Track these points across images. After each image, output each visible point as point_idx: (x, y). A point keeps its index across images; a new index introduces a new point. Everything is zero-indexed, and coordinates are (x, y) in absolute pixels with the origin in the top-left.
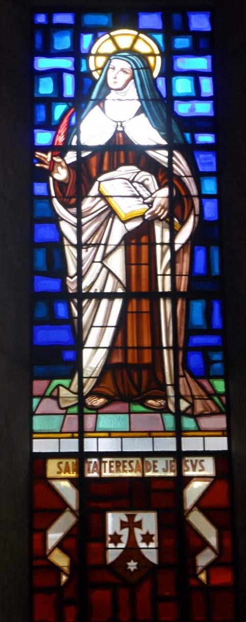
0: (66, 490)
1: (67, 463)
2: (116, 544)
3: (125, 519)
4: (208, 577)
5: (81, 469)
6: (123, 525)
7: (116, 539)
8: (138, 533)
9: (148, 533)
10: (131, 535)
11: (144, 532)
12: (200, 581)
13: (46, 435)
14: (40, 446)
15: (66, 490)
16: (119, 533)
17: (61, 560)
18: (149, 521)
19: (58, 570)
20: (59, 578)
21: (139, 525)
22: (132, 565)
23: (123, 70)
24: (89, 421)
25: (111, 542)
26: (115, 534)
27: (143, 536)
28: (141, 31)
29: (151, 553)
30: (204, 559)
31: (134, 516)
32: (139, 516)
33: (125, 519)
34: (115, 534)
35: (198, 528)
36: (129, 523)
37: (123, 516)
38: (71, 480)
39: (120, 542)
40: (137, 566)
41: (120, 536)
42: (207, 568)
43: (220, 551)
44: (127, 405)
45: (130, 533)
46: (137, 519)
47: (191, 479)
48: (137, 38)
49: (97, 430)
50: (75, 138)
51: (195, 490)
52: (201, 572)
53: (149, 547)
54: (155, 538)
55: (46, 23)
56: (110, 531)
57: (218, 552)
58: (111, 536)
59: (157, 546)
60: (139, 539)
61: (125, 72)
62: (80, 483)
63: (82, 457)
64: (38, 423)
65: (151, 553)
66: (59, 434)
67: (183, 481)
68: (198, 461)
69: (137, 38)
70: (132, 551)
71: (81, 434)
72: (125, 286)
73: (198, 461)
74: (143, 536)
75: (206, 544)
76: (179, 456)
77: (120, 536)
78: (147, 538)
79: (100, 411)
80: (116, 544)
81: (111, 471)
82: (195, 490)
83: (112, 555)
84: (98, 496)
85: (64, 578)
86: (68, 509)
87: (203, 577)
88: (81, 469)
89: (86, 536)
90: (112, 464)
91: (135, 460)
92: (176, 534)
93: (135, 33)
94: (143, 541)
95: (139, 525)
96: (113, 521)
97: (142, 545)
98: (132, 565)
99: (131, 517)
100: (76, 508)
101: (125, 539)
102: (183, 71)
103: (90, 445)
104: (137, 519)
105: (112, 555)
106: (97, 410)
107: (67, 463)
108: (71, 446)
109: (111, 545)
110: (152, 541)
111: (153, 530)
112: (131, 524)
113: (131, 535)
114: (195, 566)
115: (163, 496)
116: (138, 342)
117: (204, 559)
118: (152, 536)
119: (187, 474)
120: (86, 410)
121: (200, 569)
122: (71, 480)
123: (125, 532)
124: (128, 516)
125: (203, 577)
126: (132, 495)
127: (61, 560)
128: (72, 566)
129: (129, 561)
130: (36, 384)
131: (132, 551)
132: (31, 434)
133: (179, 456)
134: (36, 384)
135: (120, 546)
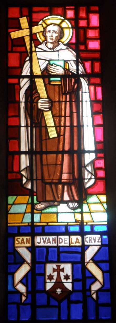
0: (27, 255)
1: (23, 239)
2: (51, 280)
3: (56, 268)
4: (97, 296)
6: (54, 270)
7: (51, 277)
8: (62, 275)
9: (67, 275)
10: (59, 275)
11: (65, 274)
12: (93, 298)
16: (52, 274)
17: (22, 288)
18: (68, 268)
19: (21, 294)
21: (63, 270)
22: (59, 291)
23: (55, 32)
26: (50, 274)
27: (64, 276)
28: (65, 18)
29: (69, 285)
30: (96, 287)
31: (60, 266)
32: (62, 266)
33: (56, 268)
34: (50, 274)
35: (98, 269)
37: (54, 266)
38: (27, 248)
39: (53, 279)
40: (61, 291)
41: (53, 276)
42: (97, 292)
45: (61, 274)
46: (61, 267)
47: (88, 246)
48: (69, 28)
49: (23, 222)
50: (27, 64)
51: (89, 254)
52: (94, 293)
53: (68, 282)
54: (71, 277)
56: (48, 274)
57: (102, 283)
58: (48, 276)
59: (71, 282)
60: (62, 277)
61: (55, 32)
62: (33, 249)
65: (69, 285)
67: (84, 248)
68: (20, 244)
69: (69, 28)
70: (59, 284)
73: (20, 244)
74: (64, 276)
77: (53, 276)
78: (67, 277)
79: (43, 211)
80: (51, 280)
82: (89, 254)
83: (49, 286)
85: (24, 298)
86: (25, 262)
87: (94, 296)
90: (66, 239)
93: (63, 18)
94: (64, 279)
95: (63, 270)
96: (50, 268)
97: (64, 281)
98: (59, 291)
99: (58, 267)
101: (55, 277)
102: (100, 67)
104: (61, 267)
105: (49, 286)
107: (23, 239)
109: (48, 281)
110: (69, 279)
111: (70, 274)
113: (59, 275)
114: (90, 290)
117: (96, 287)
118: (69, 276)
120: (35, 211)
121: (93, 292)
122: (27, 248)
123: (55, 274)
124: (57, 266)
125: (94, 296)
126: (60, 254)
127: (22, 288)
128: (27, 292)
129: (57, 289)
130: (10, 198)
134: (10, 198)
135: (52, 281)
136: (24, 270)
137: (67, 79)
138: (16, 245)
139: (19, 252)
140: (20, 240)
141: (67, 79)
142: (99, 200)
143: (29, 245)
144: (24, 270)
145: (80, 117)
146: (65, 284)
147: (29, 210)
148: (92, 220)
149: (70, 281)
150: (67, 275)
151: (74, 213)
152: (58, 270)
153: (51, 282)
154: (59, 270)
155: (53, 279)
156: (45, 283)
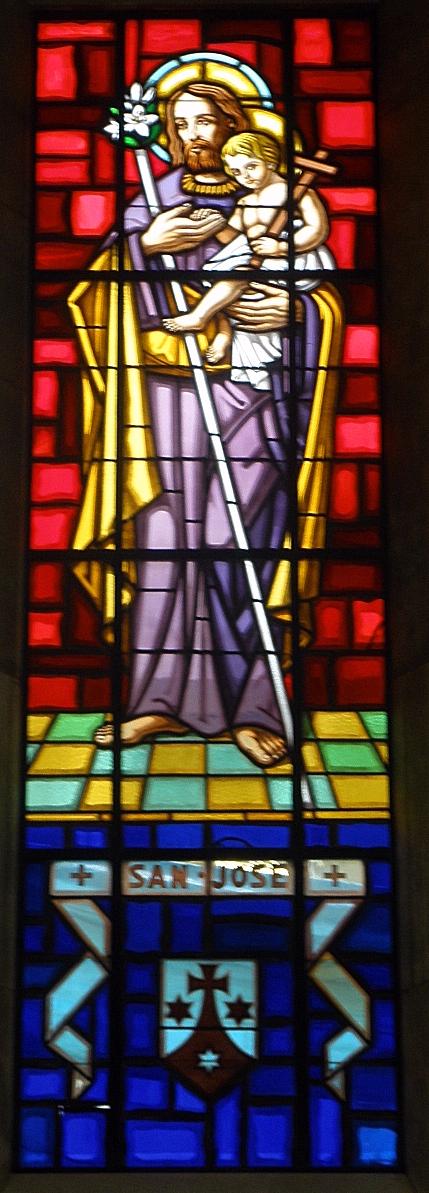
0: (93, 927)
3: (198, 974)
6: (193, 984)
8: (219, 995)
10: (209, 1006)
11: (232, 999)
15: (93, 927)
18: (241, 979)
22: (209, 1059)
30: (343, 1048)
32: (223, 969)
33: (198, 974)
41: (188, 1005)
46: (220, 973)
51: (322, 928)
60: (223, 1011)
62: (113, 905)
65: (244, 1040)
70: (209, 1032)
75: (342, 1023)
78: (238, 1010)
82: (322, 928)
84: (145, 934)
96: (176, 979)
97: (228, 1023)
101: (196, 1011)
104: (220, 973)
105: (174, 1039)
109: (170, 1022)
112: (209, 984)
113: (209, 1006)
115: (269, 930)
117: (343, 1048)
123: (196, 999)
126: (212, 928)
128: (95, 1060)
131: (209, 1032)
154: (209, 984)
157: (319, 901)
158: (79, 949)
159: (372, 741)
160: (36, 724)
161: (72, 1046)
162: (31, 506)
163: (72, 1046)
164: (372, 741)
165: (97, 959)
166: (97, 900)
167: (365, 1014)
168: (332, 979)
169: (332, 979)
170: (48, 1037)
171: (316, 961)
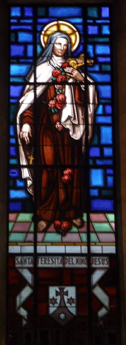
0: (28, 275)
3: (58, 290)
5: (35, 262)
6: (57, 293)
8: (66, 298)
9: (71, 298)
10: (62, 299)
11: (69, 297)
13: (16, 243)
14: (13, 249)
15: (28, 275)
16: (55, 297)
18: (71, 291)
19: (21, 317)
20: (21, 322)
21: (67, 293)
22: (62, 316)
24: (40, 237)
25: (51, 303)
26: (53, 298)
30: (102, 312)
31: (64, 289)
32: (67, 289)
33: (58, 290)
34: (53, 298)
36: (60, 292)
41: (56, 300)
43: (111, 311)
44: (79, 247)
45: (63, 298)
46: (65, 290)
51: (97, 276)
55: (47, 86)
57: (109, 309)
60: (66, 300)
62: (34, 270)
63: (36, 255)
64: (13, 237)
65: (73, 310)
66: (25, 242)
67: (91, 271)
70: (62, 307)
71: (35, 243)
72: (38, 97)
75: (102, 305)
76: (89, 256)
78: (70, 301)
81: (42, 263)
82: (97, 276)
84: (45, 278)
85: (24, 322)
88: (35, 262)
89: (39, 298)
91: (60, 258)
92: (85, 298)
96: (53, 291)
97: (68, 305)
98: (62, 316)
100: (32, 283)
101: (58, 301)
103: (41, 249)
104: (65, 290)
105: (52, 310)
106: (45, 231)
108: (30, 249)
109: (51, 305)
112: (61, 293)
113: (62, 299)
115: (80, 278)
116: (46, 144)
117: (102, 312)
119: (94, 266)
123: (59, 298)
124: (60, 289)
126: (61, 277)
128: (28, 315)
131: (62, 307)
132: (8, 243)
133: (89, 256)
136: (26, 292)
137: (76, 164)
138: (17, 266)
139: (98, 298)
140: (19, 260)
141: (76, 164)
142: (98, 238)
143: (31, 266)
144: (26, 292)
145: (89, 81)
146: (69, 309)
147: (32, 229)
148: (106, 219)
149: (74, 305)
150: (71, 298)
151: (79, 232)
152: (62, 293)
153: (54, 306)
154: (61, 293)
155: (57, 303)
156: (48, 307)
157: (95, 269)
158: (23, 283)
159: (96, 232)
160: (12, 216)
161: (23, 312)
162: (21, 253)
163: (23, 312)
164: (96, 232)
165: (30, 286)
166: (29, 269)
167: (101, 300)
168: (99, 292)
169: (99, 292)
170: (16, 309)
171: (94, 287)
